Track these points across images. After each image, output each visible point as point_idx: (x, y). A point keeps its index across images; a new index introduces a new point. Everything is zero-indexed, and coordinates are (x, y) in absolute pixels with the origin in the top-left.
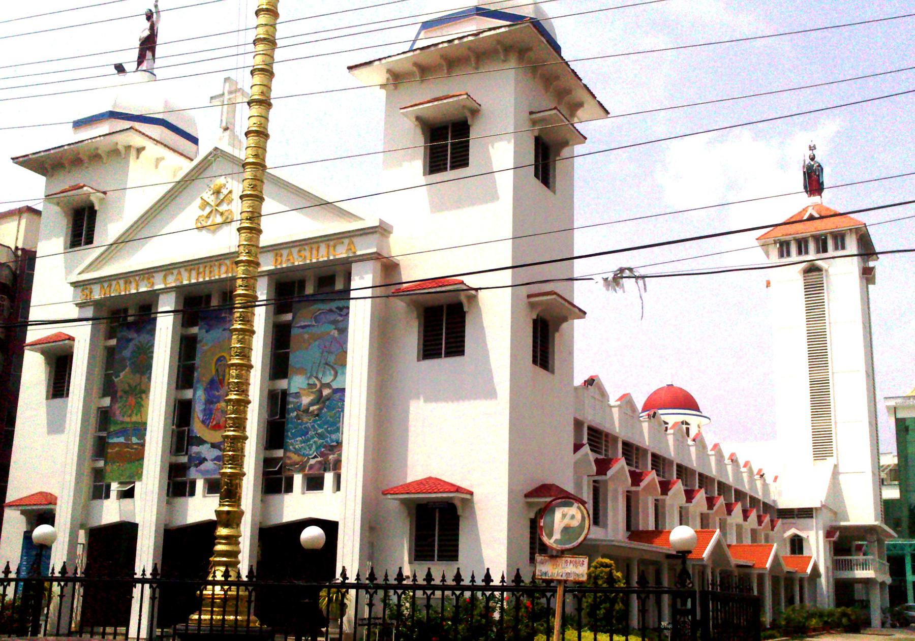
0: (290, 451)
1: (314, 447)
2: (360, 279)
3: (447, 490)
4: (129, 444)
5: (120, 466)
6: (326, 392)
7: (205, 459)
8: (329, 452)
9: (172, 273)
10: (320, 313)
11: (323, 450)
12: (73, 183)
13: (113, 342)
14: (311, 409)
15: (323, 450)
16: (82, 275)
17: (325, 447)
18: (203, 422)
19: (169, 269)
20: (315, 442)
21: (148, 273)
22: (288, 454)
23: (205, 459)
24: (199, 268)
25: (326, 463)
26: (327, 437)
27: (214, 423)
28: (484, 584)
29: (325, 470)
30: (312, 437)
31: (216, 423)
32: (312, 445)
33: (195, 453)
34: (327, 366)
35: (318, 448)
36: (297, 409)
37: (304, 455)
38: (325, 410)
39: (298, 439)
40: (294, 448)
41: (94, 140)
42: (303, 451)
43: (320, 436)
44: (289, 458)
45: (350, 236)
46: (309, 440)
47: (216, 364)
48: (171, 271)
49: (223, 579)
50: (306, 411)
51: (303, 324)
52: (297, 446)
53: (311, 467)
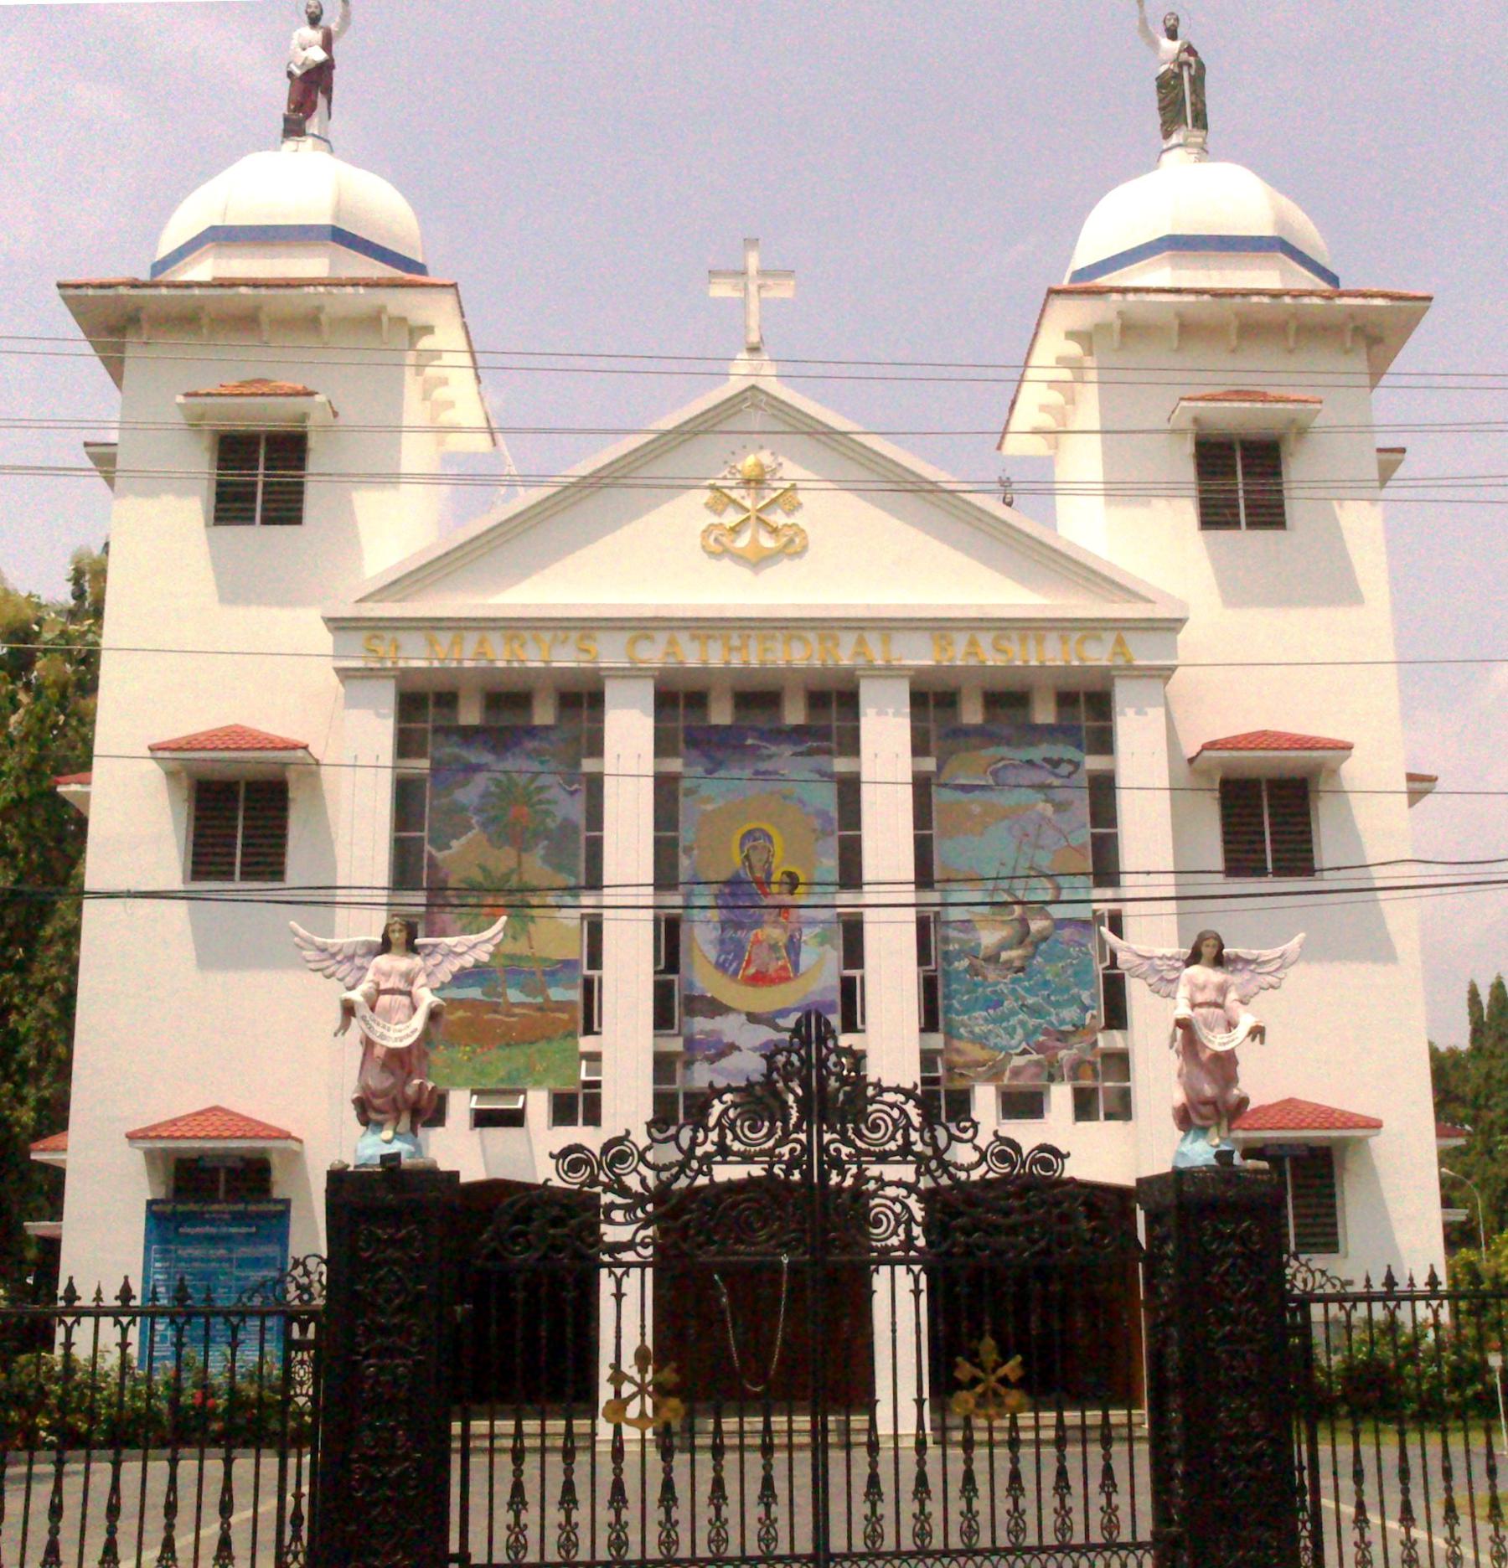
0: (960, 1038)
1: (1020, 1031)
2: (1137, 713)
3: (239, 1134)
4: (498, 1004)
5: (474, 1052)
6: (1036, 925)
7: (733, 1048)
8: (1058, 1044)
9: (1099, 639)
10: (1005, 767)
11: (1041, 1038)
12: (1247, 381)
13: (422, 765)
14: (1004, 956)
15: (1041, 1038)
16: (362, 605)
17: (1046, 1033)
18: (721, 966)
19: (1095, 629)
20: (1022, 1023)
21: (587, 627)
22: (957, 1044)
23: (733, 1048)
24: (729, 638)
25: (1051, 1065)
26: (1049, 1014)
27: (752, 971)
28: (118, 1303)
29: (1051, 1078)
30: (1013, 1013)
31: (758, 972)
32: (1014, 1028)
33: (701, 1032)
34: (937, 874)
35: (1028, 1036)
36: (972, 953)
37: (996, 1047)
38: (1039, 959)
39: (976, 1014)
40: (972, 1032)
41: (335, 290)
42: (993, 1041)
43: (1034, 1011)
44: (958, 1051)
45: (1064, 629)
46: (1005, 1018)
47: (742, 845)
48: (649, 632)
49: (1385, 1289)
50: (993, 958)
51: (963, 781)
52: (977, 1030)
53: (1016, 1073)
